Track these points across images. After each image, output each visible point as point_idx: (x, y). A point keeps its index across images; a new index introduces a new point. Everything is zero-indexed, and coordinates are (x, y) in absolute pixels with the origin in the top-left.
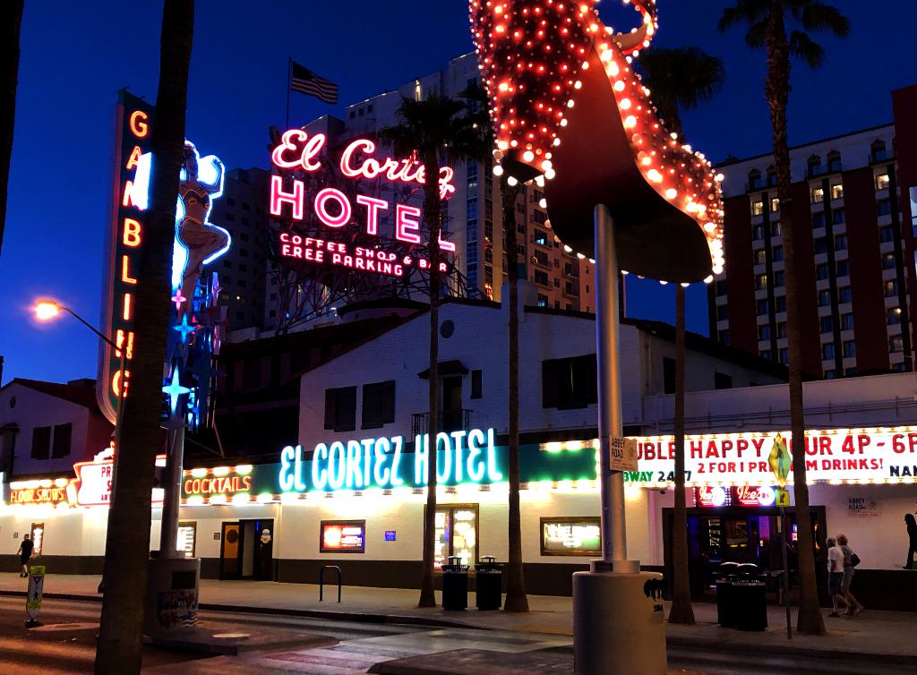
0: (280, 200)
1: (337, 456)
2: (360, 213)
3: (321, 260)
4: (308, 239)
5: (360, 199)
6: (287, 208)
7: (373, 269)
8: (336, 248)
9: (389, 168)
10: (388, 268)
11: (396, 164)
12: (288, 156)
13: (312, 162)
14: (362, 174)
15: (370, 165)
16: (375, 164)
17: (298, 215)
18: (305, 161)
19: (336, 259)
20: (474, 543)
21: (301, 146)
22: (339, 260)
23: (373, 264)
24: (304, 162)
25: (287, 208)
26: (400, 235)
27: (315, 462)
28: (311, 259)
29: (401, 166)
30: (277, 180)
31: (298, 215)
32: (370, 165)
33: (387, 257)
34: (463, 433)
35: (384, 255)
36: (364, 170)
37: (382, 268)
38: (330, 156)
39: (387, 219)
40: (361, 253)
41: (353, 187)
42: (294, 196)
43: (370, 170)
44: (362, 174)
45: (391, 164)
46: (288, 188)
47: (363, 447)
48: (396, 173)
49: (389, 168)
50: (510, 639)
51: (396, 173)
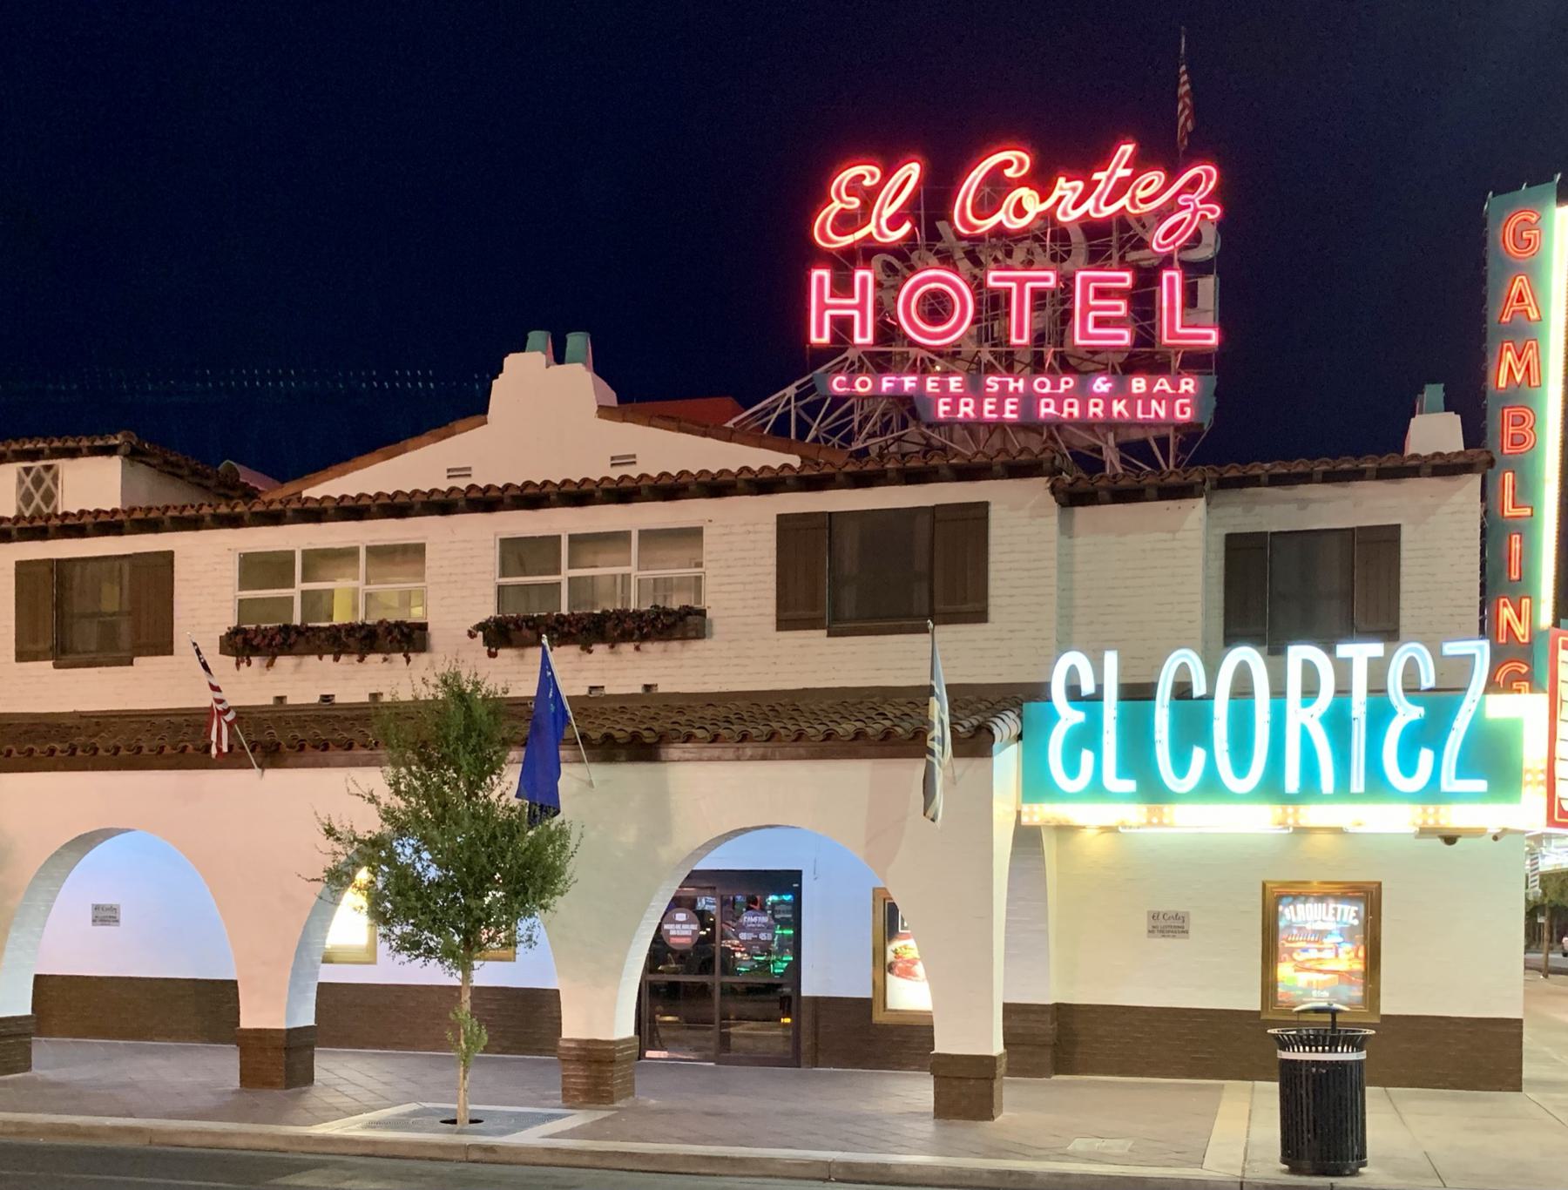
0: (828, 313)
1: (1242, 689)
2: (993, 305)
3: (1014, 416)
4: (885, 379)
5: (993, 279)
6: (843, 327)
7: (1126, 414)
8: (944, 386)
9: (1061, 199)
10: (1159, 410)
11: (1080, 185)
12: (846, 222)
13: (894, 223)
14: (1000, 223)
15: (1020, 201)
16: (1028, 196)
17: (863, 337)
18: (881, 228)
19: (1046, 410)
20: (1544, 765)
21: (870, 198)
22: (1051, 410)
23: (1126, 407)
24: (878, 226)
25: (843, 327)
26: (1173, 334)
27: (1162, 710)
28: (994, 416)
29: (1090, 187)
30: (821, 276)
31: (863, 337)
32: (1020, 201)
33: (1055, 386)
34: (1376, 649)
35: (1048, 383)
36: (1003, 217)
37: (1146, 410)
38: (931, 205)
39: (1056, 308)
40: (996, 387)
41: (975, 252)
42: (856, 301)
43: (1020, 211)
44: (1000, 223)
45: (1066, 189)
46: (842, 286)
47: (1343, 670)
48: (1076, 206)
49: (1061, 199)
50: (572, 1130)
51: (1076, 206)
